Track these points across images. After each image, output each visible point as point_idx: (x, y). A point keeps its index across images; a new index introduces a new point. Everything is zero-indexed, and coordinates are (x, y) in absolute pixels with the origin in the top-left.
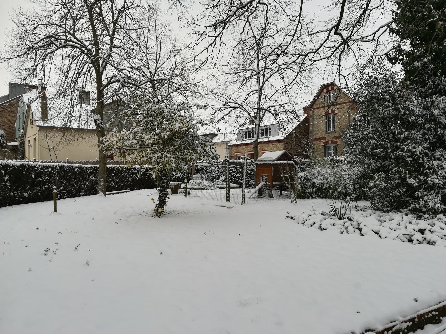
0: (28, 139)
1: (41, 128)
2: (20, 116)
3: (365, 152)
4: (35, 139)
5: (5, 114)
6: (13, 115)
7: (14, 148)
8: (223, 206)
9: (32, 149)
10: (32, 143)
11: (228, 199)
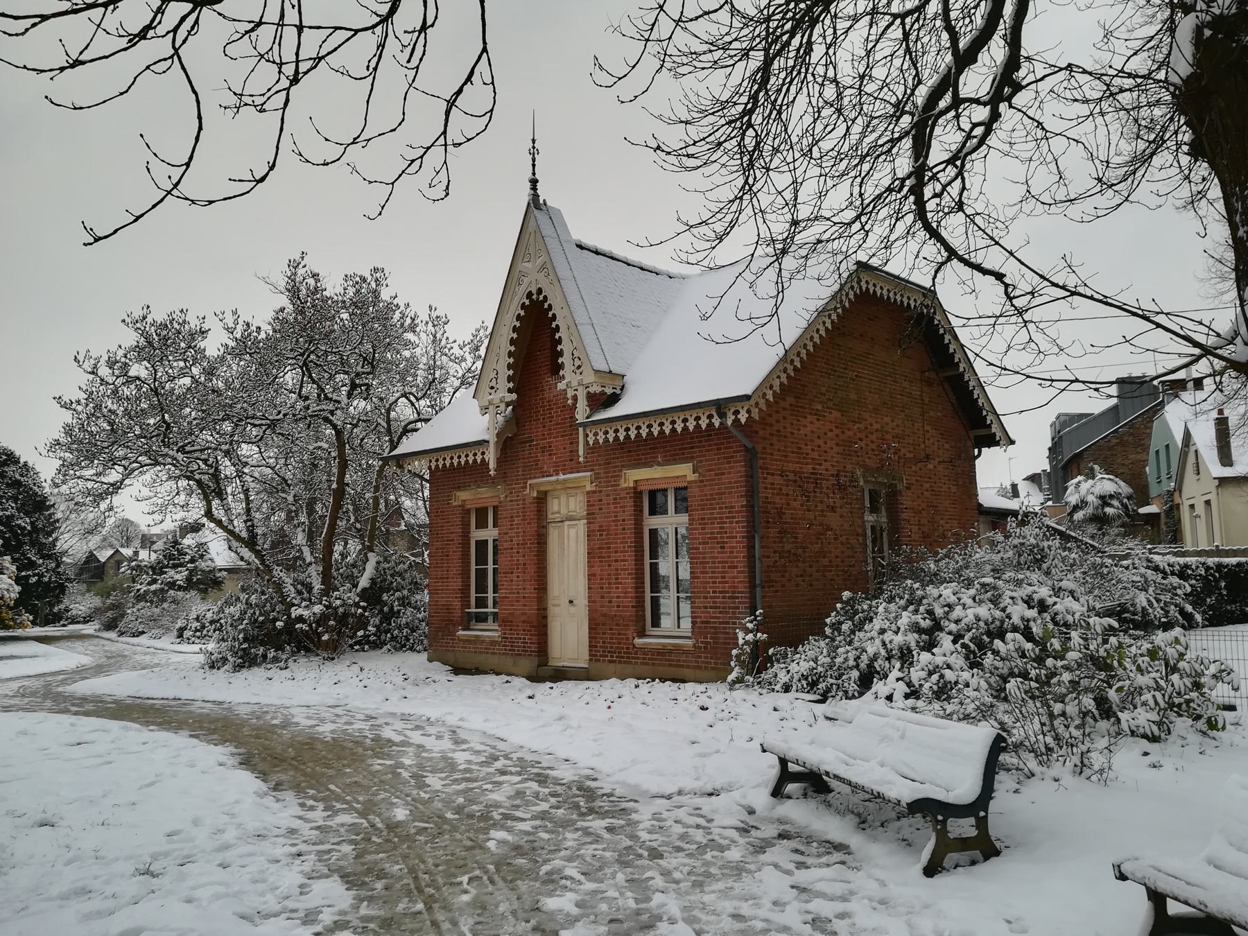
0: (1187, 503)
1: (1223, 481)
2: (1157, 452)
3: (771, 651)
4: (1208, 503)
5: (1123, 449)
6: (1139, 450)
7: (1152, 519)
8: (240, 181)
9: (1201, 525)
10: (1200, 509)
11: (235, 313)
